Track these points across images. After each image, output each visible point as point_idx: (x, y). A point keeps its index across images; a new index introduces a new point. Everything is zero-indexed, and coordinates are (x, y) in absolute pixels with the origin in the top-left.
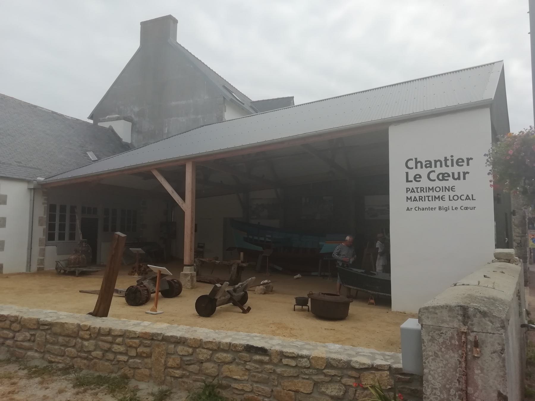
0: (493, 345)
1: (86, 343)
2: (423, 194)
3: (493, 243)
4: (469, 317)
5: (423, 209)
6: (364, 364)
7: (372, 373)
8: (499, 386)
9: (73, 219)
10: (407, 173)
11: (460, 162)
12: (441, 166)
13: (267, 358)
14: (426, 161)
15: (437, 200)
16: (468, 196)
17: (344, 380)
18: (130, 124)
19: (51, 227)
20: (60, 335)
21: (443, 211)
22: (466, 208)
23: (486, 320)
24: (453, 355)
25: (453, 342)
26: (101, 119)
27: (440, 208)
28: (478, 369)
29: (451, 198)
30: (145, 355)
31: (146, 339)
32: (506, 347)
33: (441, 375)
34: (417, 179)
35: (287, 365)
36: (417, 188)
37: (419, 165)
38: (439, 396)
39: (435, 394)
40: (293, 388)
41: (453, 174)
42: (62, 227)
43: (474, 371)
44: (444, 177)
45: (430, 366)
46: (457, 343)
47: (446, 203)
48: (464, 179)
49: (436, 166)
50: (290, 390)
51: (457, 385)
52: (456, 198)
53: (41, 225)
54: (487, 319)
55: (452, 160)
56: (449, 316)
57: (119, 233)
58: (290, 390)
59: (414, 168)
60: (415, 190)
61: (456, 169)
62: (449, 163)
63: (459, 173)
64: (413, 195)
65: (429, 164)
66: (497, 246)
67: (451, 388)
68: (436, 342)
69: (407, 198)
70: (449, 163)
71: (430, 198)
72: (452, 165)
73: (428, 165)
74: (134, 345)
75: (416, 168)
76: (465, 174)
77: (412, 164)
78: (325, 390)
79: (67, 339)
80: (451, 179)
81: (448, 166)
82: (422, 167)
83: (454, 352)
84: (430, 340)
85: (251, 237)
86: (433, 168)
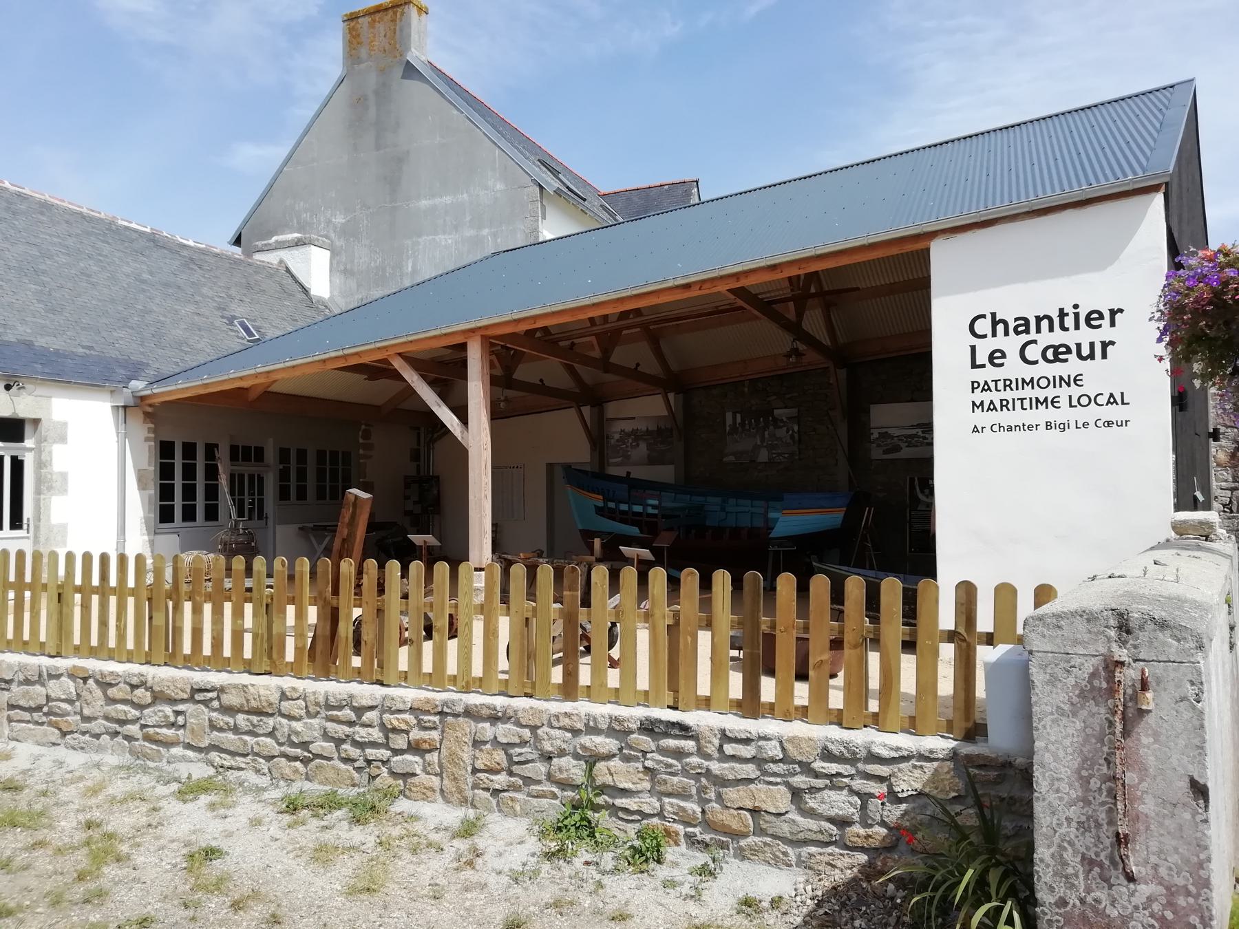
0: (1178, 686)
1: (297, 726)
2: (1009, 395)
3: (1171, 501)
4: (1128, 632)
5: (1010, 429)
6: (898, 749)
7: (915, 767)
8: (1191, 767)
9: (212, 473)
10: (973, 348)
11: (1093, 319)
12: (1051, 329)
13: (690, 745)
14: (1016, 320)
15: (1042, 408)
16: (1112, 395)
17: (858, 784)
18: (328, 253)
19: (166, 493)
20: (240, 711)
21: (1055, 432)
22: (1109, 424)
23: (1165, 637)
24: (1095, 709)
25: (1096, 683)
26: (260, 243)
27: (1048, 426)
28: (1147, 736)
29: (1074, 402)
30: (426, 746)
31: (428, 713)
32: (1205, 688)
33: (1070, 750)
34: (1093, 323)
35: (733, 756)
36: (996, 381)
37: (1000, 327)
38: (1068, 794)
39: (1058, 791)
40: (749, 805)
41: (1079, 346)
42: (189, 493)
43: (1139, 740)
44: (1057, 353)
45: (1049, 734)
46: (1104, 685)
47: (1063, 414)
48: (1104, 356)
49: (1038, 330)
50: (740, 808)
51: (1105, 769)
52: (1084, 401)
53: (144, 489)
54: (1168, 633)
55: (1077, 315)
56: (1090, 632)
57: (354, 491)
58: (740, 808)
59: (990, 334)
60: (992, 385)
61: (1085, 336)
62: (1069, 322)
63: (1092, 345)
64: (987, 397)
65: (1023, 325)
66: (1178, 508)
67: (1091, 776)
68: (1060, 685)
69: (974, 403)
70: (1069, 322)
71: (1026, 404)
72: (1077, 327)
73: (1020, 329)
74: (403, 726)
75: (994, 335)
76: (1105, 345)
77: (983, 326)
78: (815, 806)
79: (255, 719)
80: (1073, 357)
81: (1067, 329)
82: (1006, 334)
83: (1097, 705)
84: (1049, 682)
85: (611, 505)
86: (1033, 335)
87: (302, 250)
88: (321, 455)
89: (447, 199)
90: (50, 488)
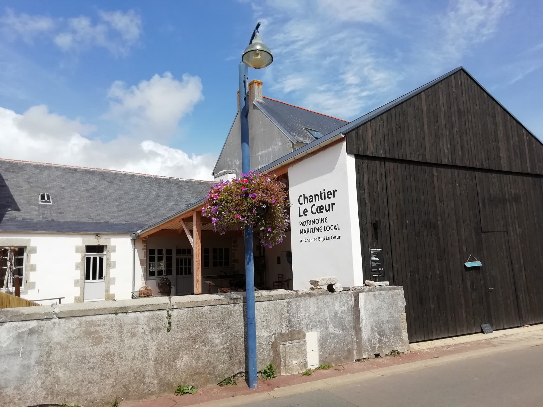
22: (335, 238)
44: (320, 209)
76: (333, 204)
87: (226, 175)
88: (215, 250)
89: (266, 151)
90: (110, 266)
